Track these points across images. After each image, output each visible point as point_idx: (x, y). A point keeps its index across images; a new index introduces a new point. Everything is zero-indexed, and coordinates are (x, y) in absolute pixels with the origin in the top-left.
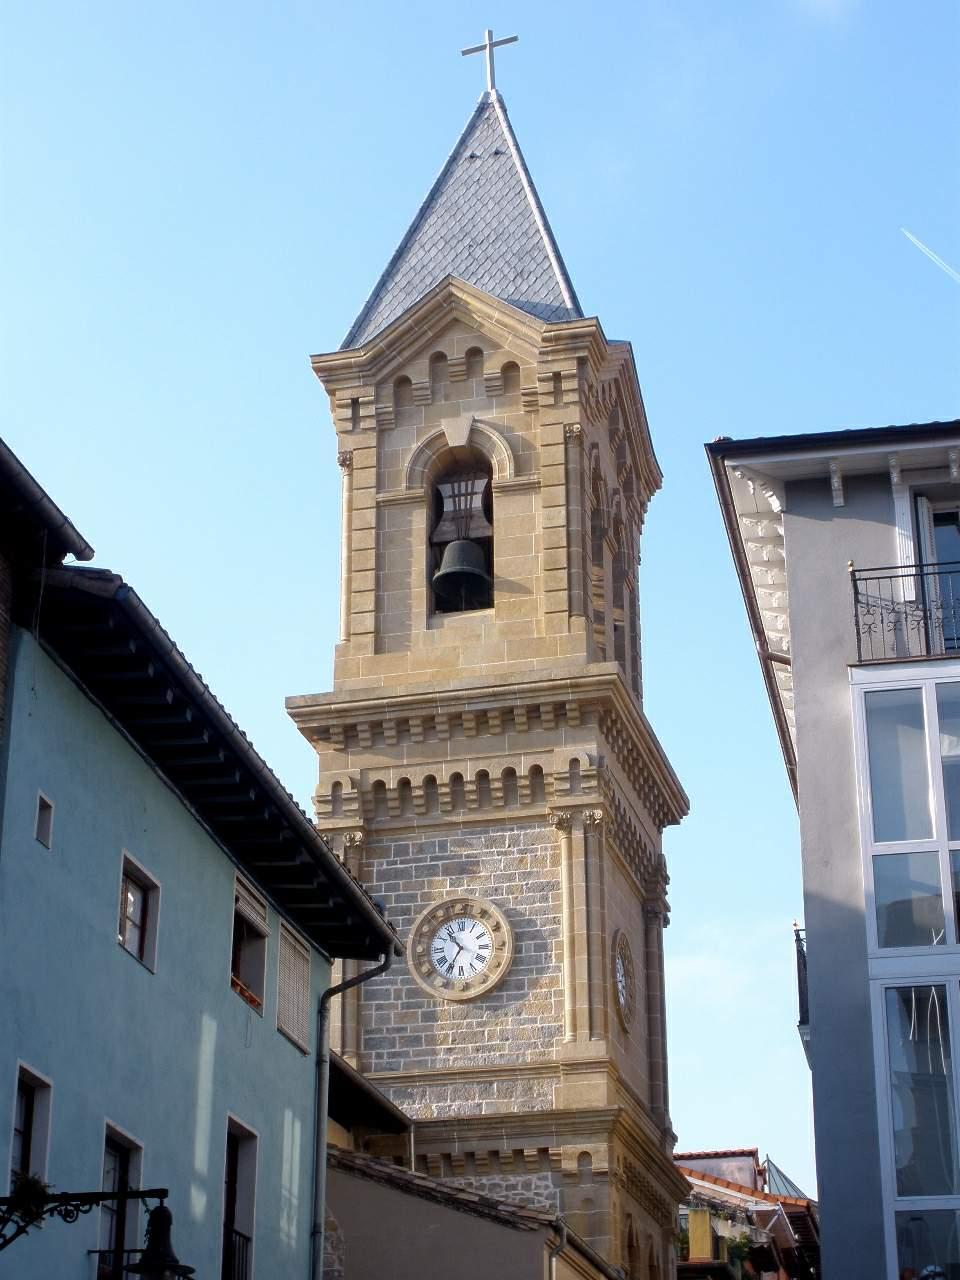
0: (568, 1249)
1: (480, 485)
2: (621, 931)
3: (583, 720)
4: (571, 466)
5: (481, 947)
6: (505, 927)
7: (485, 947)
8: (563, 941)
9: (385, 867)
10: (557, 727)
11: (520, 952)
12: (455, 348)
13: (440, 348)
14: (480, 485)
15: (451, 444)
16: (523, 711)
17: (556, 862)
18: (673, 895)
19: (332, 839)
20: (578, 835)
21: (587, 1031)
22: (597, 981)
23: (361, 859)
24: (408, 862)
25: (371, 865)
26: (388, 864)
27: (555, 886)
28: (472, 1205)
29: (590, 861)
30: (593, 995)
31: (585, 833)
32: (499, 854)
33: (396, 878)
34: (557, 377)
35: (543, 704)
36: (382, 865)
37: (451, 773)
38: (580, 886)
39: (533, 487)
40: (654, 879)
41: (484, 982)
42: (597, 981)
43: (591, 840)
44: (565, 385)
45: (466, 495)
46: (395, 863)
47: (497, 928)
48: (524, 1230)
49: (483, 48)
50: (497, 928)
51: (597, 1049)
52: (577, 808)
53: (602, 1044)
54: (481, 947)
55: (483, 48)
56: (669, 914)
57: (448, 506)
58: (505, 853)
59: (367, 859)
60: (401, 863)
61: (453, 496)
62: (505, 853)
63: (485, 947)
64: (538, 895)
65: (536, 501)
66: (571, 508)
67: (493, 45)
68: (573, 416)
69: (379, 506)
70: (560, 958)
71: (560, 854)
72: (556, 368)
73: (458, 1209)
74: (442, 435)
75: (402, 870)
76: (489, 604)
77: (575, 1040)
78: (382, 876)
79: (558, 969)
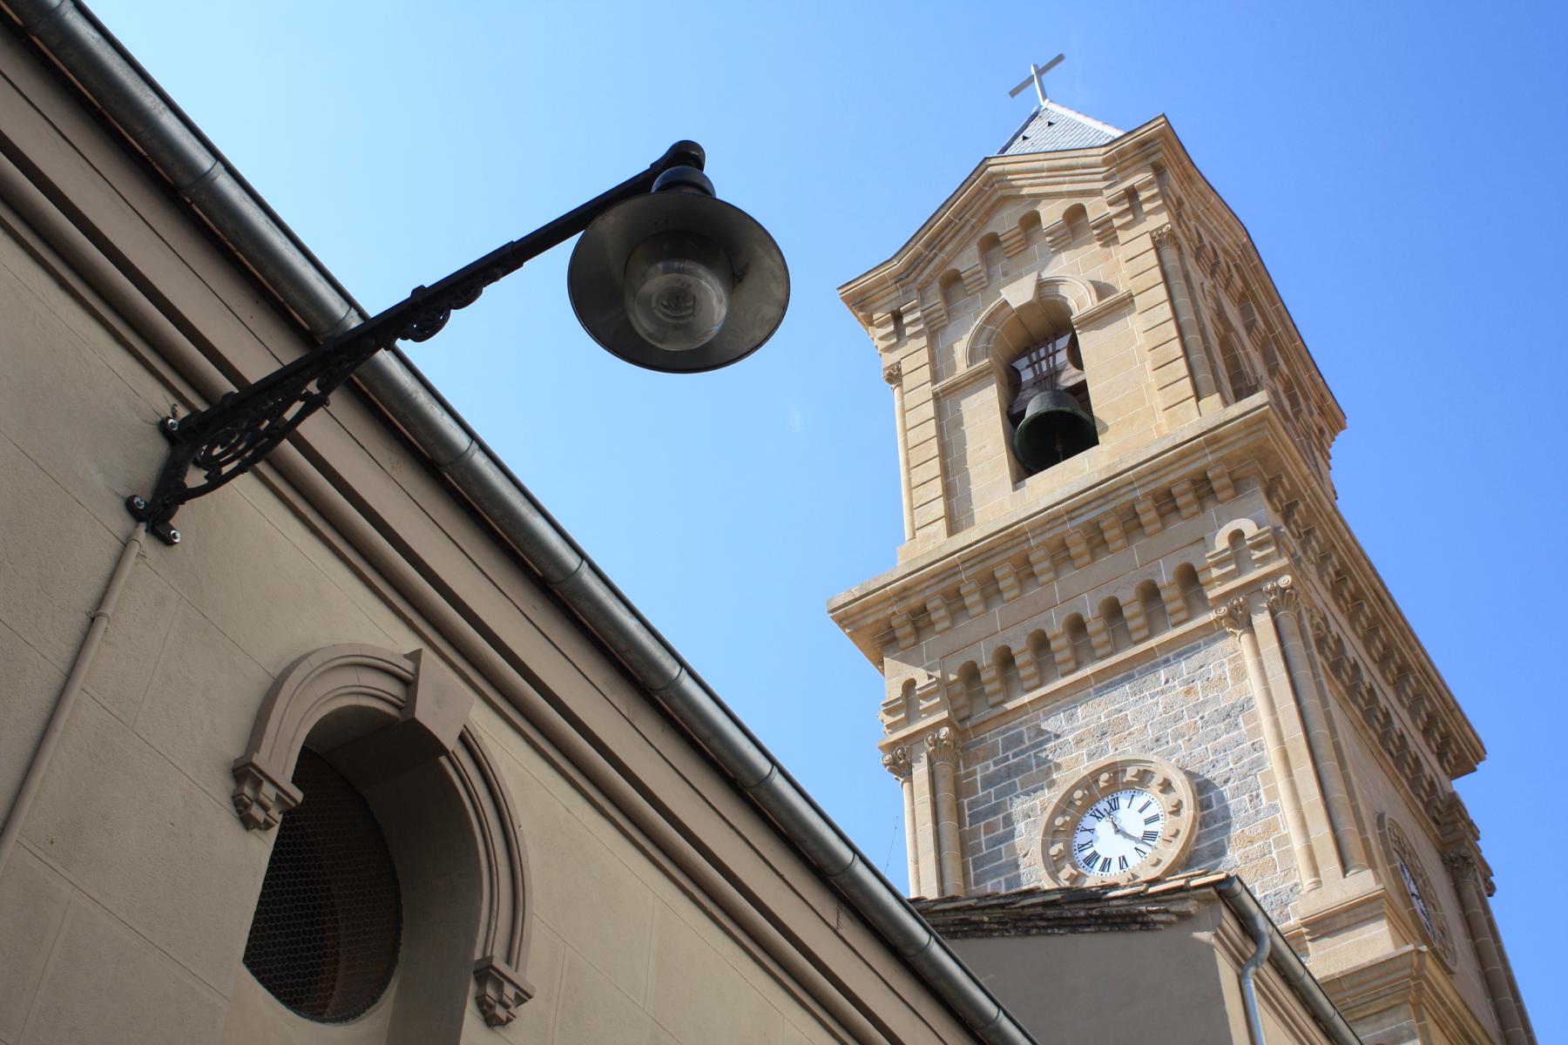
0: (1267, 971)
1: (1063, 342)
2: (1386, 817)
3: (1238, 485)
4: (1183, 319)
5: (1148, 822)
6: (1188, 812)
7: (1155, 818)
8: (1272, 771)
9: (992, 769)
10: (1202, 509)
11: (1209, 806)
12: (1005, 223)
13: (989, 230)
14: (1063, 342)
15: (1015, 305)
16: (1149, 503)
17: (1239, 674)
18: (1489, 847)
19: (910, 750)
20: (1262, 621)
21: (1337, 866)
22: (1320, 730)
23: (957, 767)
24: (1023, 752)
25: (974, 773)
26: (996, 764)
27: (1246, 706)
28: (1052, 913)
29: (1288, 645)
30: (1335, 815)
31: (1273, 614)
32: (1152, 696)
33: (1009, 777)
34: (1132, 194)
35: (1173, 482)
36: (987, 768)
37: (1063, 618)
38: (1296, 740)
39: (1126, 303)
40: (1449, 819)
41: (1155, 865)
42: (1320, 730)
43: (1283, 621)
44: (1143, 195)
45: (1046, 358)
46: (1007, 758)
47: (1177, 810)
48: (1168, 924)
49: (1031, 79)
50: (1177, 810)
51: (1363, 883)
52: (1253, 587)
53: (1368, 875)
54: (1148, 822)
55: (1031, 79)
56: (1463, 787)
57: (1027, 375)
58: (1163, 692)
59: (966, 767)
60: (1015, 755)
61: (1031, 365)
62: (1163, 692)
63: (1155, 818)
64: (1222, 726)
65: (1133, 324)
66: (1193, 357)
67: (1040, 72)
68: (1162, 220)
69: (936, 397)
70: (1272, 793)
71: (1244, 665)
72: (1127, 184)
73: (1027, 933)
74: (1006, 303)
75: (1018, 765)
76: (1096, 443)
77: (1318, 884)
78: (989, 782)
79: (1275, 808)
